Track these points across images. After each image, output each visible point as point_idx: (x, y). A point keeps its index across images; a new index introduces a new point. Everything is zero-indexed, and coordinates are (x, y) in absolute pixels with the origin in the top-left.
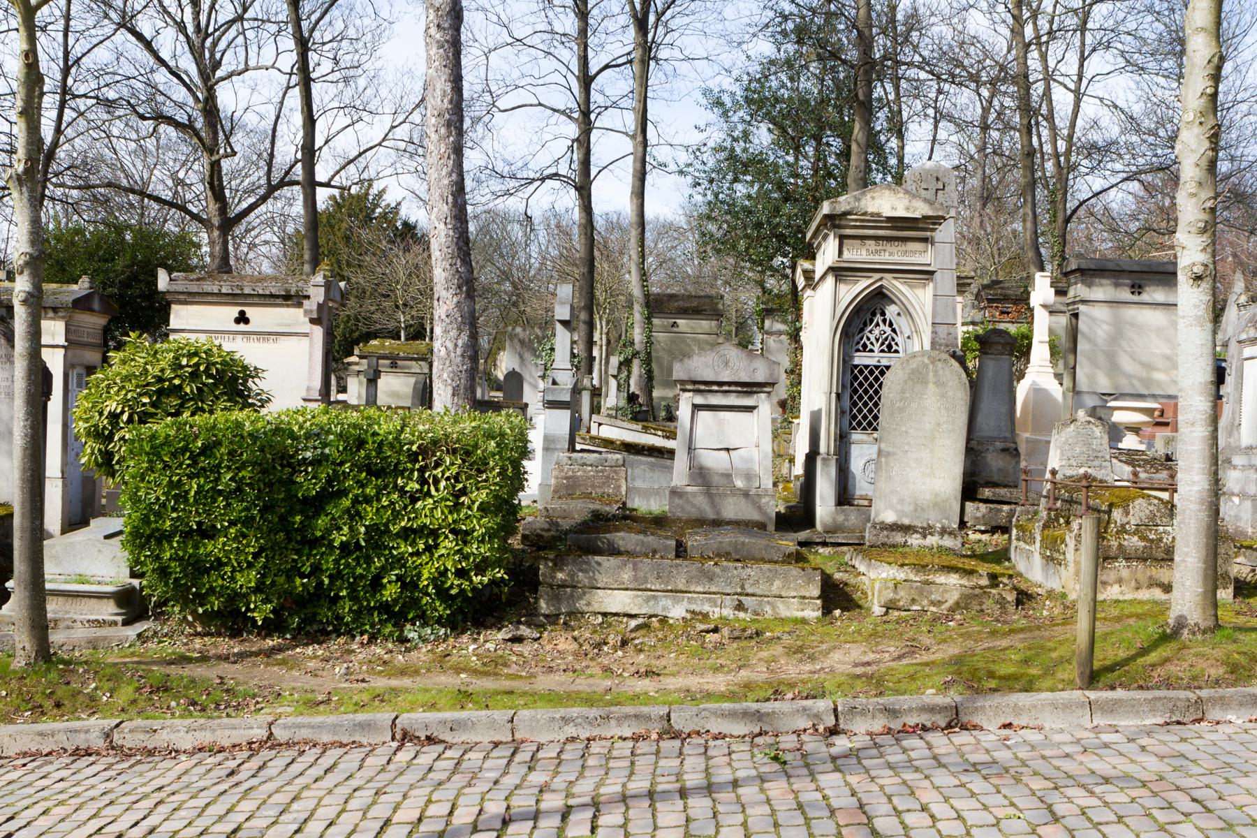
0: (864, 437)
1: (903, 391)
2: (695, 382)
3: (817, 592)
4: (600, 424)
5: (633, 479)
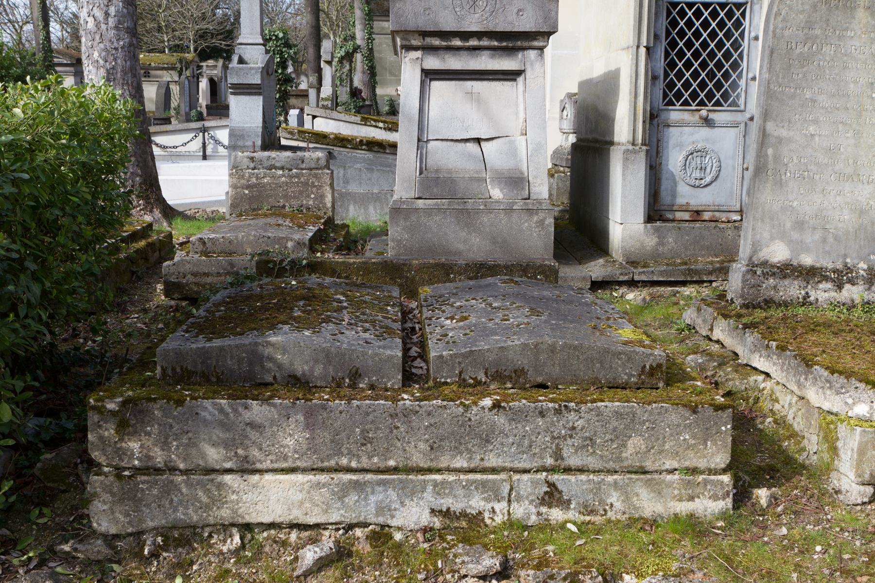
0: (686, 116)
1: (809, 25)
2: (424, 34)
3: (721, 459)
4: (314, 117)
5: (346, 182)
